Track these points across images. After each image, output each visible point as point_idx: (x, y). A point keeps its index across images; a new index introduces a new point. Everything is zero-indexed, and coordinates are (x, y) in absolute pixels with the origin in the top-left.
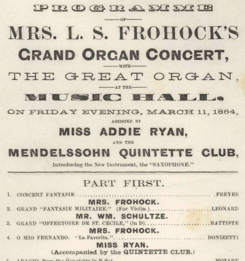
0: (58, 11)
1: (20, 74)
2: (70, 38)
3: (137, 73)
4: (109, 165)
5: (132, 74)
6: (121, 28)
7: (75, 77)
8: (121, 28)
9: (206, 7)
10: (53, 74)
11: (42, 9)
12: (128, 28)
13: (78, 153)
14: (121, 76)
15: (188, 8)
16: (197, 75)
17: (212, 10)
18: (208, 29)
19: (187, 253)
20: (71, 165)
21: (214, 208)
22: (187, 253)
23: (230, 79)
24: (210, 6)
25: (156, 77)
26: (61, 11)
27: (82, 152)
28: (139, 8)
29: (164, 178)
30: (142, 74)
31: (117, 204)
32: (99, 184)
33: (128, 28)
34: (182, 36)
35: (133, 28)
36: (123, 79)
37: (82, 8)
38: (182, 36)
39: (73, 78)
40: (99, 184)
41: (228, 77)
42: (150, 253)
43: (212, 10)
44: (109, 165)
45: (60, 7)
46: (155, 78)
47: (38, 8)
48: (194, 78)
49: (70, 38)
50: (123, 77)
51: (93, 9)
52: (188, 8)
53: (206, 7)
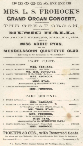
12: (43, 10)
37: (28, 3)
47: (13, 3)
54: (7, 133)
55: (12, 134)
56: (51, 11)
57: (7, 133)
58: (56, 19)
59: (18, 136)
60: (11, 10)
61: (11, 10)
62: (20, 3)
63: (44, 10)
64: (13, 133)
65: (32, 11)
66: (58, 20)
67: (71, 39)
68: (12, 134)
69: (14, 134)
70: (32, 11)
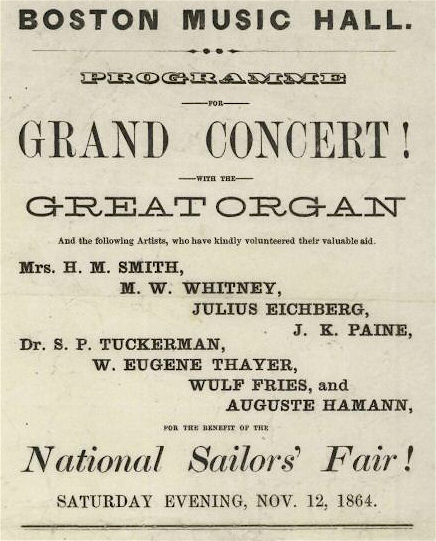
0: (200, 82)
1: (204, 199)
3: (190, 199)
5: (176, 199)
7: (54, 208)
9: (335, 78)
10: (134, 199)
11: (95, 81)
12: (331, 124)
13: (252, 309)
14: (344, 205)
15: (309, 78)
16: (320, 204)
17: (344, 82)
18: (311, 129)
23: (395, 215)
24: (342, 76)
25: (31, 208)
26: (122, 82)
28: (236, 79)
30: (204, 199)
33: (331, 124)
35: (341, 125)
36: (349, 212)
37: (153, 78)
39: (50, 210)
41: (390, 211)
42: (306, 409)
43: (344, 82)
45: (203, 75)
46: (30, 212)
47: (89, 78)
48: (50, 210)
50: (350, 208)
51: (143, 80)
52: (309, 78)
53: (335, 78)
54: (285, 307)
55: (146, 348)
56: (274, 502)
57: (285, 311)
58: (160, 367)
59: (254, 309)
60: (57, 124)
61: (57, 124)
62: (120, 75)
63: (339, 128)
64: (150, 344)
65: (196, 456)
66: (142, 27)
67: (219, 84)
68: (146, 348)
69: (154, 348)
70: (196, 456)
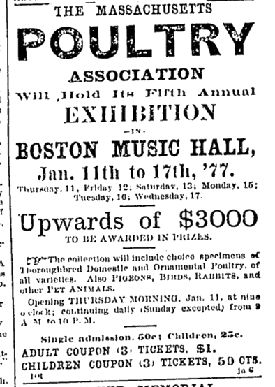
2: (68, 120)
4: (135, 259)
6: (68, 109)
8: (68, 109)
12: (77, 108)
19: (202, 141)
20: (174, 277)
21: (114, 109)
22: (202, 141)
27: (105, 75)
29: (39, 345)
31: (259, 272)
32: (208, 277)
33: (77, 108)
34: (186, 116)
38: (186, 116)
40: (208, 277)
44: (135, 259)
49: (68, 120)
